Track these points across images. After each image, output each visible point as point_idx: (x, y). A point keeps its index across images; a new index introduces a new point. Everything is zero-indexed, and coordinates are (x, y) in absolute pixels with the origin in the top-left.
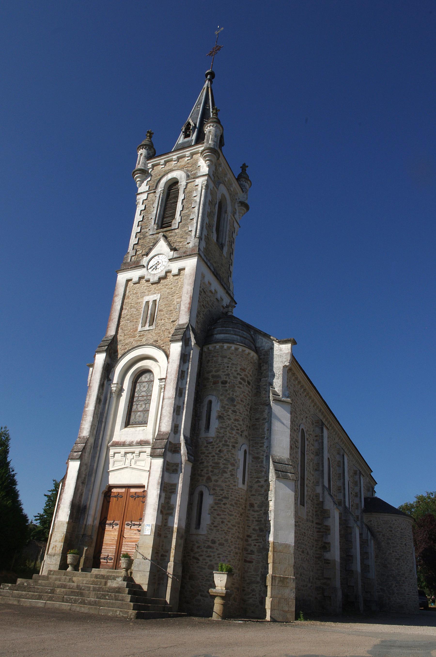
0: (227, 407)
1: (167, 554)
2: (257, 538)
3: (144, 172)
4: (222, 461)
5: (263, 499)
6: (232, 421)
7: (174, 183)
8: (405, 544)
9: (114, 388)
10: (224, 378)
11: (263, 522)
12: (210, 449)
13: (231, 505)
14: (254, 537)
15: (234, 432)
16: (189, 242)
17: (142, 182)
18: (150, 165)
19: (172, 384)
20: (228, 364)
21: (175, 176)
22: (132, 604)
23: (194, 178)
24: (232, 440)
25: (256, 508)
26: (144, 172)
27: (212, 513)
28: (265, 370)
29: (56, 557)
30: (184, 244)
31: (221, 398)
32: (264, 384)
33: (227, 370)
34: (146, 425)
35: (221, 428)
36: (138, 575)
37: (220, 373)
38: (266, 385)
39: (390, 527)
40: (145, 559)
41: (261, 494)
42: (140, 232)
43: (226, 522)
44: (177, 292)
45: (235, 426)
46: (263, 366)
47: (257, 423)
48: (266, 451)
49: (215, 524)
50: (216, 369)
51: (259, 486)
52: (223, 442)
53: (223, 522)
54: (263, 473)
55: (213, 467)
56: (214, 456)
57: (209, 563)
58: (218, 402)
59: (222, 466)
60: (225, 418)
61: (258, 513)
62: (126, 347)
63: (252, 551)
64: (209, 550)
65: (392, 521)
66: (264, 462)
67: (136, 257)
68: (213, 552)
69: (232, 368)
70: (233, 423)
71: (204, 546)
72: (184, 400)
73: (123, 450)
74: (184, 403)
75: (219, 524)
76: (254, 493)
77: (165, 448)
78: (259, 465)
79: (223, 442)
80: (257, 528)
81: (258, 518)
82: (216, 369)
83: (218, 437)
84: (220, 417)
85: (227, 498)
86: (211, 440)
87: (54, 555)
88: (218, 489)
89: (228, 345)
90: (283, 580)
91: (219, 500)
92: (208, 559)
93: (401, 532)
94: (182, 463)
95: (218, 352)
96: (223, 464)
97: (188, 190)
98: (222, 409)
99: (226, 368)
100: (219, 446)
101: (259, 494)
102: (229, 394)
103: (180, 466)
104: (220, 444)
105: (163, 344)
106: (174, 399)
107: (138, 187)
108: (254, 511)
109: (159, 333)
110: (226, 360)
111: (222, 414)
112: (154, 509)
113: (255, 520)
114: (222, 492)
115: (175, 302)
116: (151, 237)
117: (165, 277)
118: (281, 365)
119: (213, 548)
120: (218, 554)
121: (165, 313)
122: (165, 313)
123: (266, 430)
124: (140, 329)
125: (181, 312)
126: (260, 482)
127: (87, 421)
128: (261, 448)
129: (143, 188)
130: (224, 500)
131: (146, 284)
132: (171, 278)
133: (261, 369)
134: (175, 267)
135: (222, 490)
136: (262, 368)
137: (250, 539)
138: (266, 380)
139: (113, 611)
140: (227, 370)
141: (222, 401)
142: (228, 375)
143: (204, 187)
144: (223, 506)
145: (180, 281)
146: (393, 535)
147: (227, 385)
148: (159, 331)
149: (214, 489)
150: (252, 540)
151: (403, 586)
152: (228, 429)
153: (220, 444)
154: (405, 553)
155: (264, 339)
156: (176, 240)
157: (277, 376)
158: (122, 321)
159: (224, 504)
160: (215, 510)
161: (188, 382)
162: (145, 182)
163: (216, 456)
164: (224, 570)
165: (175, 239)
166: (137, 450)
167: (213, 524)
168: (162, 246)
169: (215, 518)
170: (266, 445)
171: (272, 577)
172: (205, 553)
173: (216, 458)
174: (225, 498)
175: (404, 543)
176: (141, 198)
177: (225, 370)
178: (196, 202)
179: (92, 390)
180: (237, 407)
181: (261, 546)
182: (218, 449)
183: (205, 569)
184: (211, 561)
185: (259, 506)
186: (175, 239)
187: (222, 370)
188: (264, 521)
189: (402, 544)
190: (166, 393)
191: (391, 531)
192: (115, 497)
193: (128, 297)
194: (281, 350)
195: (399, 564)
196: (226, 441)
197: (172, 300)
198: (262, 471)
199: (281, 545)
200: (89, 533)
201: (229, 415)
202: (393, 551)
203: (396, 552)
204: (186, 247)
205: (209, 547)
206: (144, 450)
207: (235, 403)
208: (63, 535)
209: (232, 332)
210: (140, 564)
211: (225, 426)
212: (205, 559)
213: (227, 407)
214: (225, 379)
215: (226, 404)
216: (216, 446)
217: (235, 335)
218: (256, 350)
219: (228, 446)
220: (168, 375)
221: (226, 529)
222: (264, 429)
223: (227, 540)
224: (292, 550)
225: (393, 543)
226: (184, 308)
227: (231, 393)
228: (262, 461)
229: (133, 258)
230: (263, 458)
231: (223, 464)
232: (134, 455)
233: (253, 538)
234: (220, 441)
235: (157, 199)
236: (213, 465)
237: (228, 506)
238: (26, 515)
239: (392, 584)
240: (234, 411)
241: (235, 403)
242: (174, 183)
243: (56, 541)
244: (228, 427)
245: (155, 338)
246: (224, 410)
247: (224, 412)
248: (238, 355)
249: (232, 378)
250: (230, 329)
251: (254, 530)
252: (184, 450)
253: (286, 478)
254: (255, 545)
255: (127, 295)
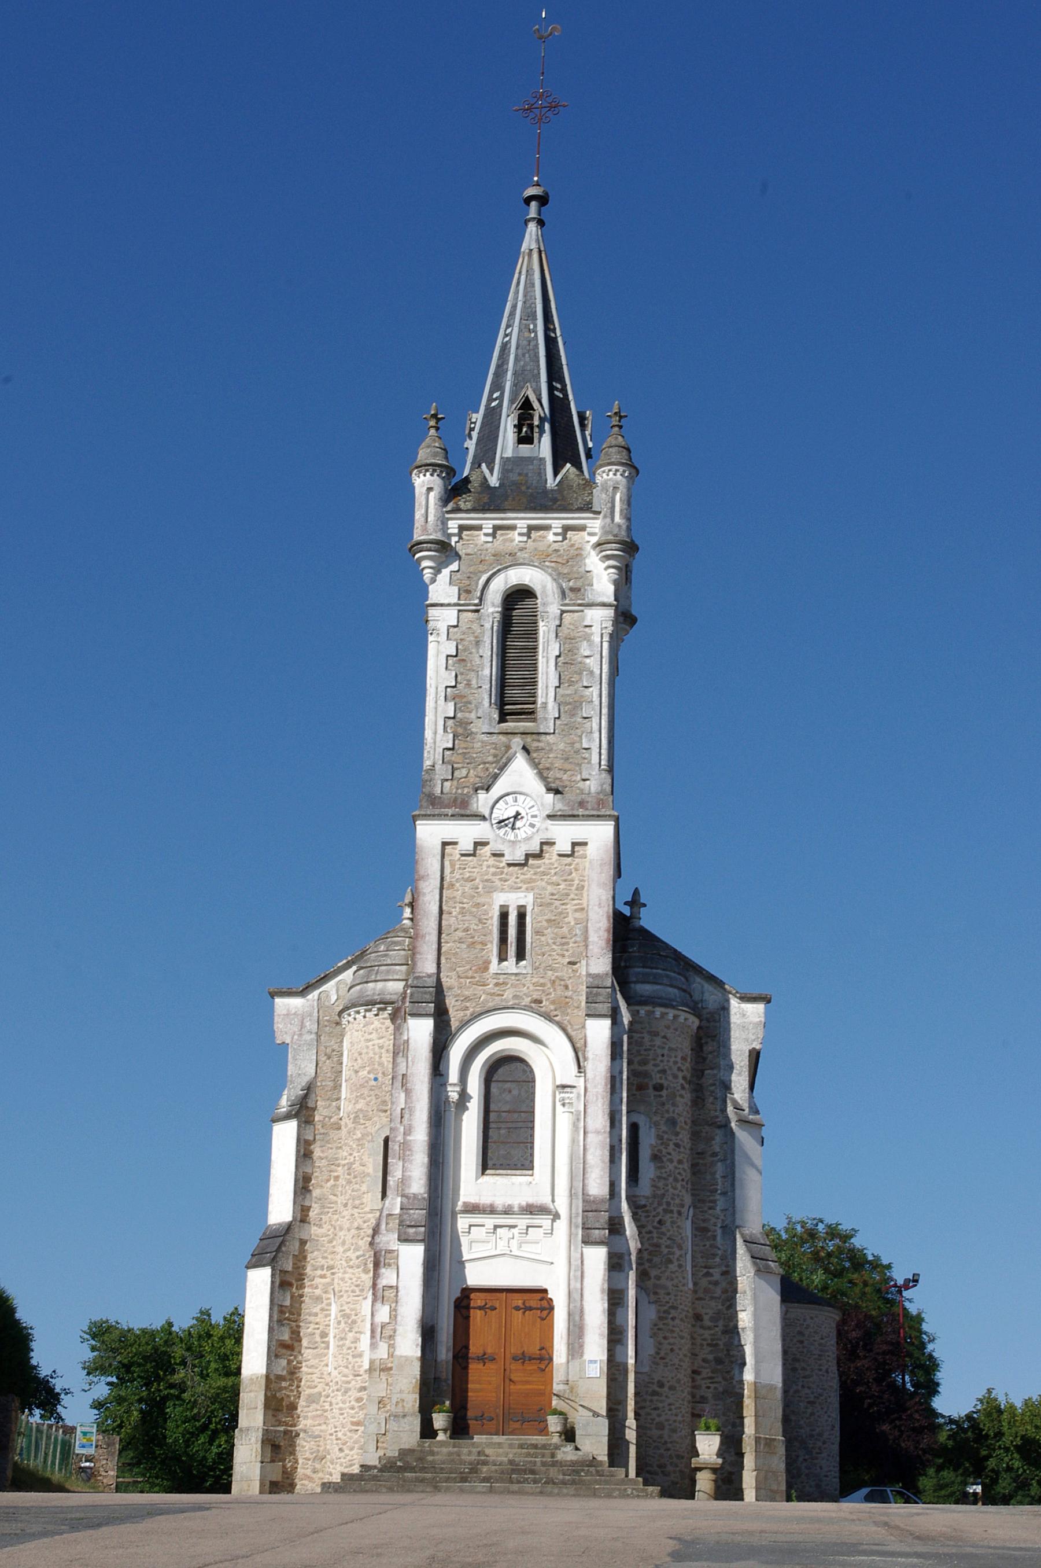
0: (666, 1136)
1: (620, 1407)
2: (710, 1375)
3: (445, 550)
4: (664, 1242)
5: (720, 1307)
6: (675, 1163)
7: (519, 597)
8: (827, 1372)
9: (454, 1095)
10: (657, 1079)
11: (722, 1347)
12: (643, 1219)
13: (682, 1320)
14: (706, 1372)
15: (679, 1185)
16: (587, 777)
17: (437, 571)
18: (453, 526)
19: (600, 1105)
20: (664, 1048)
21: (526, 581)
22: (640, 1479)
23: (580, 605)
24: (677, 1201)
25: (707, 1323)
26: (445, 550)
27: (655, 1334)
28: (711, 1053)
29: (409, 1418)
30: (574, 778)
31: (655, 1119)
32: (711, 1081)
33: (662, 1061)
34: (530, 1172)
35: (659, 1178)
36: (587, 1442)
37: (649, 1067)
38: (714, 1085)
39: (800, 1333)
40: (596, 1414)
41: (716, 1298)
42: (454, 718)
43: (677, 1351)
44: (572, 896)
45: (679, 1173)
46: (706, 1043)
47: (701, 1161)
48: (722, 1217)
49: (662, 1354)
50: (639, 1058)
51: (710, 1283)
52: (665, 1206)
53: (672, 1350)
54: (718, 1259)
55: (650, 1253)
56: (650, 1232)
57: (658, 1419)
58: (650, 1127)
59: (665, 1251)
60: (665, 1159)
61: (712, 1332)
62: (468, 1004)
63: (702, 1397)
64: (655, 1398)
65: (805, 1320)
66: (719, 1238)
67: (455, 782)
68: (661, 1401)
69: (671, 1057)
70: (676, 1168)
71: (647, 1392)
72: (621, 1135)
73: (490, 1221)
74: (621, 1140)
75: (666, 1354)
76: (702, 1295)
77: (601, 1225)
78: (708, 1243)
79: (665, 1206)
80: (710, 1357)
81: (712, 1340)
82: (639, 1058)
83: (654, 1196)
84: (655, 1158)
85: (674, 1308)
86: (643, 1203)
87: (404, 1416)
88: (662, 1292)
89: (663, 1010)
90: (769, 1442)
91: (665, 1312)
92: (654, 1413)
93: (820, 1345)
94: (630, 1254)
95: (641, 1023)
96: (667, 1247)
97: (564, 631)
98: (659, 1142)
99: (660, 1058)
100: (658, 1214)
101: (712, 1298)
102: (668, 1111)
103: (626, 1258)
104: (660, 1210)
105: (556, 1010)
106: (607, 1135)
107: (427, 581)
108: (702, 1327)
109: (543, 985)
110: (658, 1041)
111: (659, 1151)
112: (601, 1335)
113: (705, 1343)
114: (667, 1298)
115: (570, 919)
116: (485, 738)
117: (539, 856)
118: (746, 1049)
119: (661, 1395)
120: (670, 1405)
121: (551, 941)
122: (551, 941)
123: (718, 1176)
124: (494, 966)
125: (590, 947)
126: (712, 1275)
127: (414, 1163)
128: (711, 1212)
129: (442, 589)
130: (672, 1311)
131: (492, 861)
132: (554, 860)
133: (702, 1051)
134: (564, 834)
135: (669, 1294)
136: (705, 1048)
137: (698, 1377)
138: (715, 1075)
139: (619, 1490)
140: (662, 1061)
141: (656, 1124)
142: (664, 1071)
143: (606, 638)
144: (671, 1323)
145: (576, 870)
146: (805, 1350)
147: (664, 1093)
148: (542, 981)
149: (656, 1293)
150: (703, 1379)
151: (817, 1458)
152: (671, 1179)
153: (660, 1210)
154: (824, 1389)
155: (706, 986)
156: (552, 764)
157: (737, 1067)
158: (447, 942)
159: (673, 1319)
160: (659, 1329)
161: (625, 1100)
162: (446, 572)
163: (655, 1231)
164: (713, 1429)
165: (549, 760)
166: (522, 1222)
167: (658, 1353)
168: (520, 773)
169: (660, 1344)
170: (721, 1204)
171: (757, 1440)
172: (648, 1403)
173: (655, 1235)
174: (674, 1308)
175: (824, 1368)
176: (442, 619)
177: (658, 1062)
178: (592, 673)
179: (414, 1098)
180: (681, 1136)
181: (721, 1389)
182: (657, 1219)
183: (650, 1429)
184: (659, 1416)
185: (712, 1319)
186: (549, 760)
187: (652, 1062)
188: (724, 1345)
189: (820, 1370)
190: (589, 1120)
191: (802, 1342)
192: (480, 1308)
193: (452, 885)
194: (744, 1015)
195: (812, 1414)
196: (668, 1204)
197: (563, 914)
198: (714, 1255)
199: (765, 1386)
200: (444, 1376)
201: (669, 1154)
202: (803, 1386)
203: (809, 1388)
204: (579, 788)
205: (654, 1393)
206: (536, 1222)
207: (678, 1129)
208: (414, 1381)
209: (665, 981)
210: (588, 1424)
211: (664, 1175)
212: (649, 1414)
213: (666, 1136)
214: (659, 1081)
215: (664, 1132)
216: (654, 1213)
217: (671, 986)
218: (696, 1008)
219: (672, 1212)
220: (588, 1086)
221: (676, 1361)
222: (715, 1173)
223: (678, 1381)
224: (779, 1394)
225: (804, 1369)
226: (596, 939)
227: (671, 1109)
228: (714, 1237)
229: (447, 784)
230: (715, 1231)
231: (667, 1247)
232: (515, 1231)
233: (704, 1375)
234: (660, 1204)
235: (488, 634)
236: (651, 1249)
237: (677, 1321)
238: (938, 1384)
239: (798, 1456)
240: (677, 1145)
241: (678, 1129)
242: (519, 597)
243: (401, 1392)
244: (669, 1176)
245: (536, 996)
246: (662, 1144)
247: (662, 1148)
248: (676, 1030)
249: (670, 1078)
250: (659, 971)
251: (704, 1360)
252: (632, 1230)
253: (768, 1271)
254: (709, 1388)
255: (447, 879)
